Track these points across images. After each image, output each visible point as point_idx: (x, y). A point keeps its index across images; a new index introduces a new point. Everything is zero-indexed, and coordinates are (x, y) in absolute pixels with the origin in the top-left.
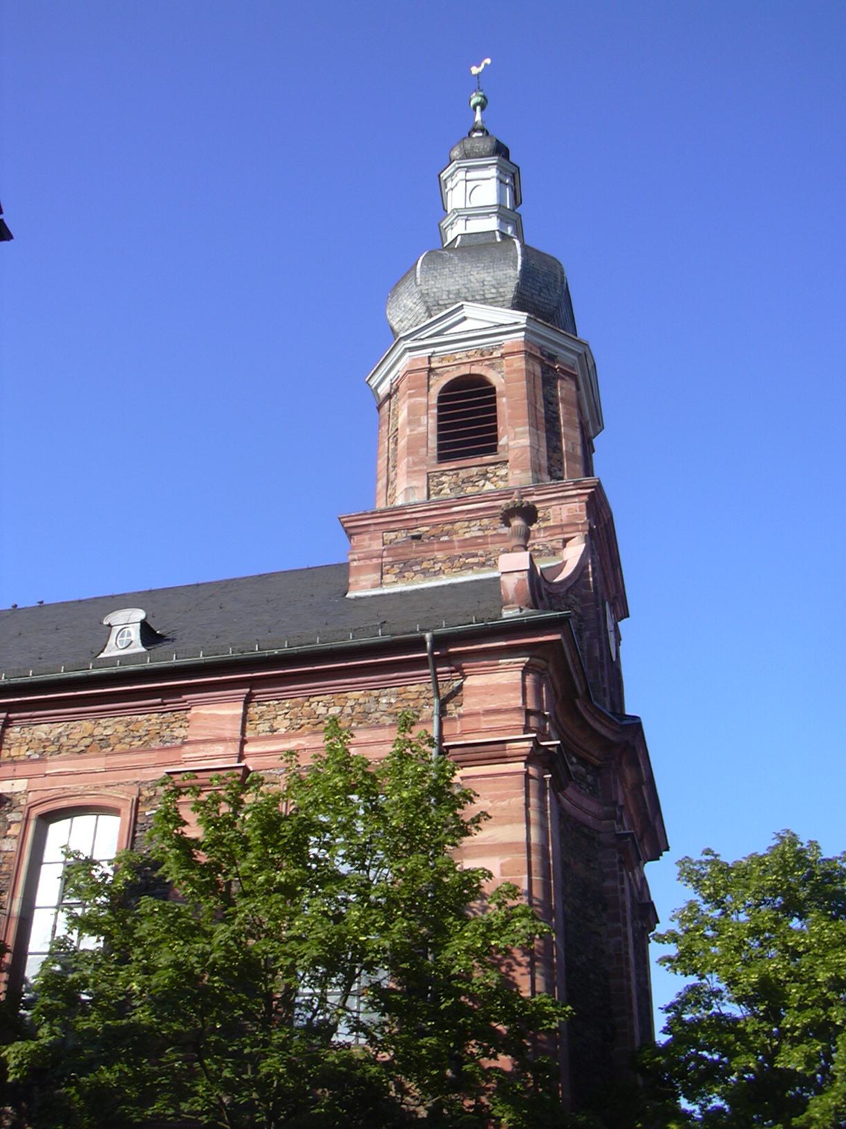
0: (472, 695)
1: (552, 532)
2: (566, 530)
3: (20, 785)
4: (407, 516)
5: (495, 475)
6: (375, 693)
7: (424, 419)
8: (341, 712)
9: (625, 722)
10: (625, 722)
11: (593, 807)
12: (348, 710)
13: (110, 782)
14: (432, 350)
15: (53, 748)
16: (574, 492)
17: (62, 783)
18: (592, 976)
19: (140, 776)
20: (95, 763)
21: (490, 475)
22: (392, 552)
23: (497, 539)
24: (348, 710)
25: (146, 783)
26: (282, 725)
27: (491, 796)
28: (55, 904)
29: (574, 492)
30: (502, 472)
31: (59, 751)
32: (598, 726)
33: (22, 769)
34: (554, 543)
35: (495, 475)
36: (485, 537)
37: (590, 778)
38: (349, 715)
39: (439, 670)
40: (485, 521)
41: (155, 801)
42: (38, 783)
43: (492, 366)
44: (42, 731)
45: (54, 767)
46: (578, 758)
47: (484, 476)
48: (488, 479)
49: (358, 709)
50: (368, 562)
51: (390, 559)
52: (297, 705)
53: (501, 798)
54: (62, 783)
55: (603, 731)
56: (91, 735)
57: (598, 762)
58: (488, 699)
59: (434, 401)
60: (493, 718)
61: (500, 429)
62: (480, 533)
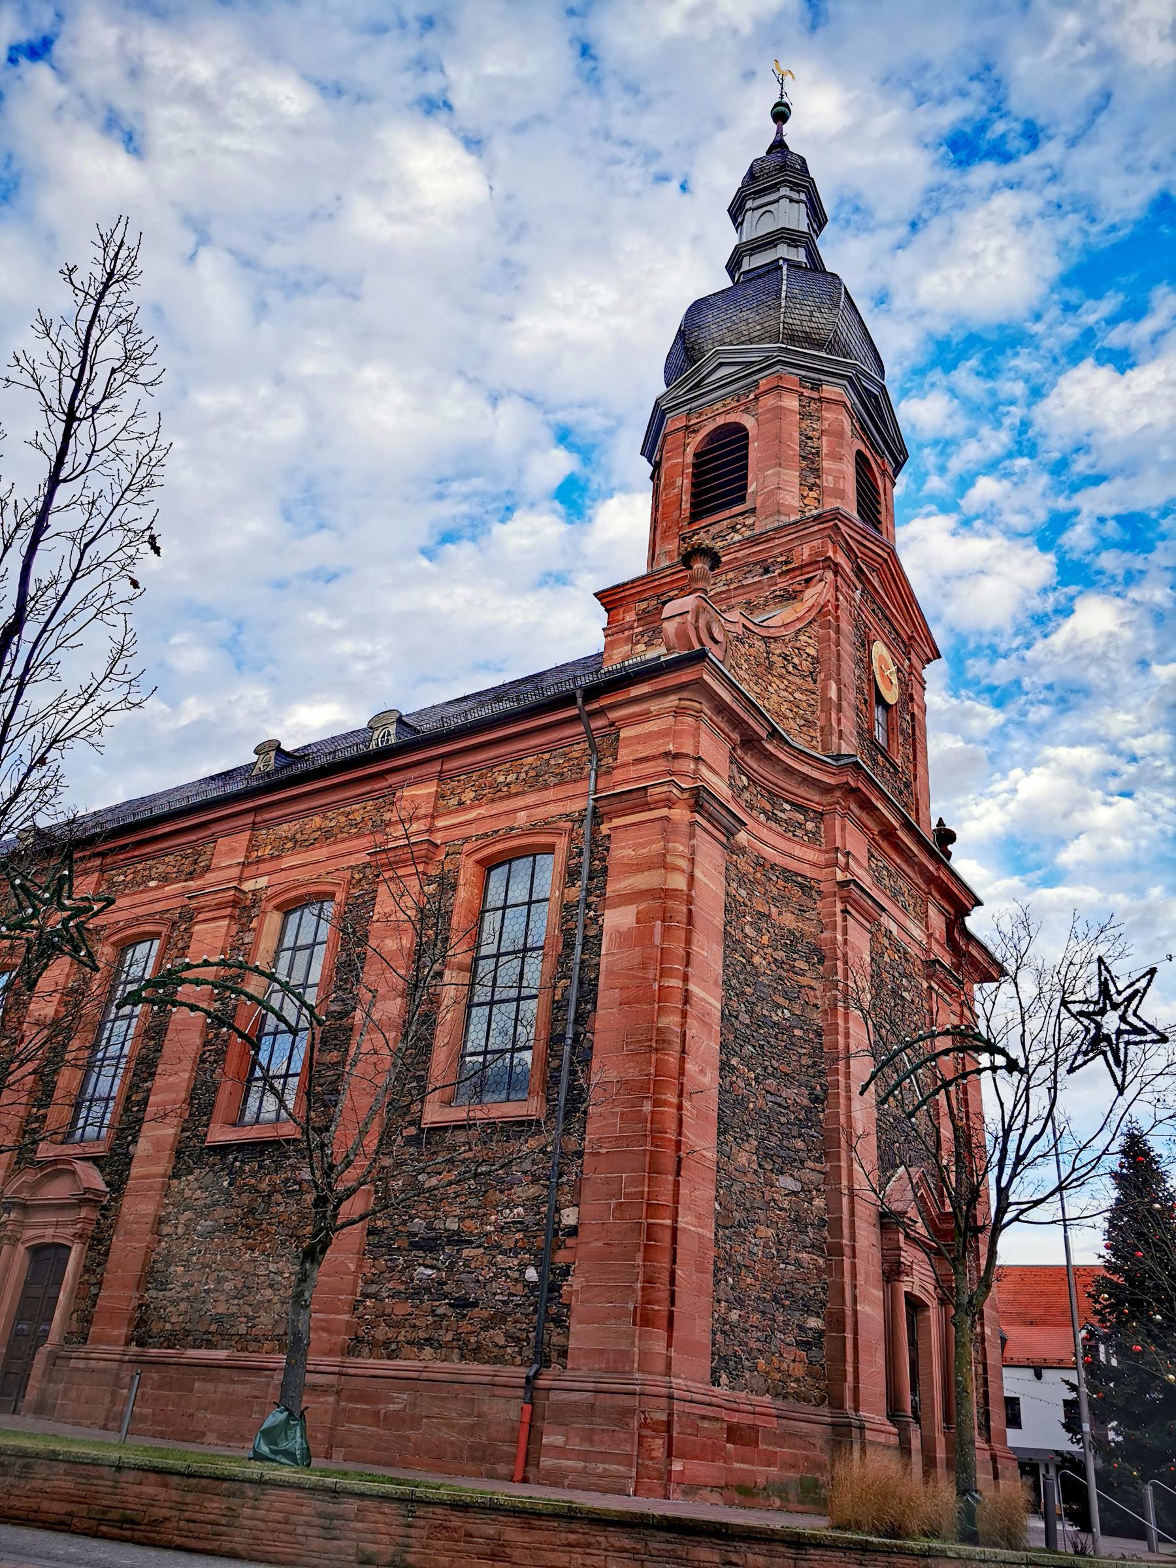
0: (627, 746)
1: (792, 575)
2: (805, 570)
3: (262, 882)
4: (657, 583)
5: (744, 526)
6: (547, 756)
7: (679, 482)
8: (517, 779)
9: (842, 762)
10: (842, 762)
11: (811, 855)
12: (523, 776)
13: (330, 869)
14: (688, 407)
15: (290, 845)
16: (816, 528)
17: (295, 875)
18: (797, 1032)
19: (353, 860)
20: (321, 853)
21: (739, 526)
22: (642, 622)
23: (741, 591)
24: (523, 776)
25: (358, 866)
26: (468, 796)
27: (634, 845)
28: (1116, 1092)
29: (816, 528)
30: (749, 522)
31: (294, 848)
32: (806, 769)
33: (264, 867)
34: (795, 586)
35: (744, 526)
36: (729, 590)
37: (810, 826)
38: (524, 780)
39: (593, 726)
40: (731, 575)
41: (363, 883)
42: (276, 878)
43: (746, 411)
44: (284, 829)
45: (286, 863)
46: (792, 804)
47: (734, 529)
48: (736, 531)
49: (532, 773)
50: (621, 635)
51: (641, 629)
52: (481, 777)
53: (643, 845)
54: (295, 875)
55: (815, 774)
56: (320, 829)
57: (820, 809)
58: (640, 748)
59: (689, 459)
60: (641, 766)
61: (750, 478)
62: (726, 588)
